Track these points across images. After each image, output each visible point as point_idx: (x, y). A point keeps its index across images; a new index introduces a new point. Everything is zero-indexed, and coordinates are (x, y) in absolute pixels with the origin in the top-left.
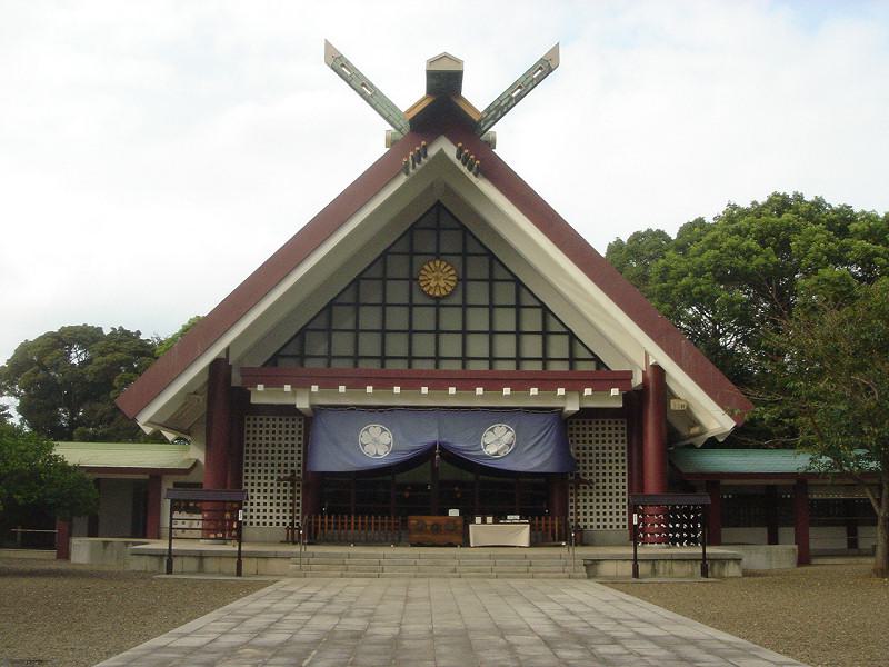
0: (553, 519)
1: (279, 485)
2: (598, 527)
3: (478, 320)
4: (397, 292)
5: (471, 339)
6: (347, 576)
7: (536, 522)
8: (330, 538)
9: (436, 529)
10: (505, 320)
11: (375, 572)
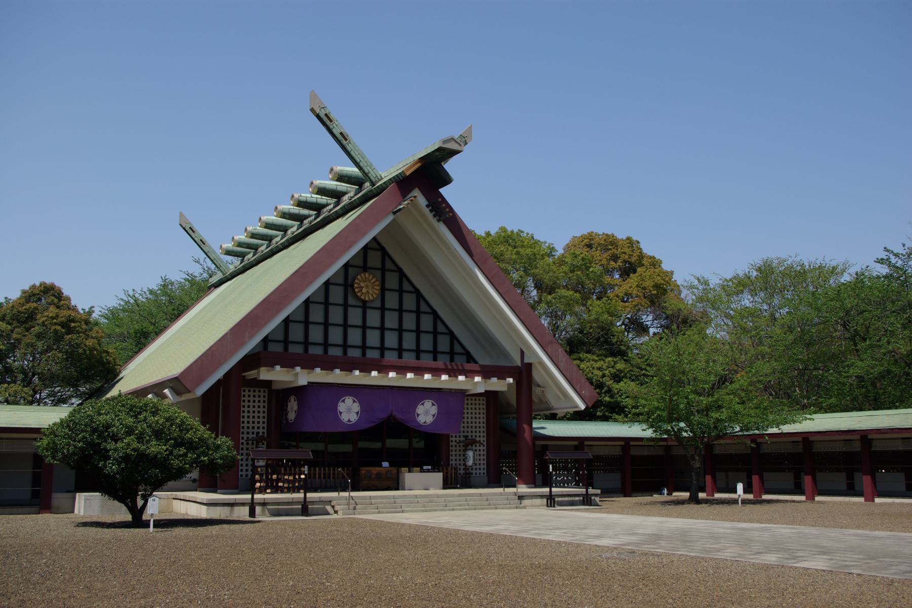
1: (248, 444)
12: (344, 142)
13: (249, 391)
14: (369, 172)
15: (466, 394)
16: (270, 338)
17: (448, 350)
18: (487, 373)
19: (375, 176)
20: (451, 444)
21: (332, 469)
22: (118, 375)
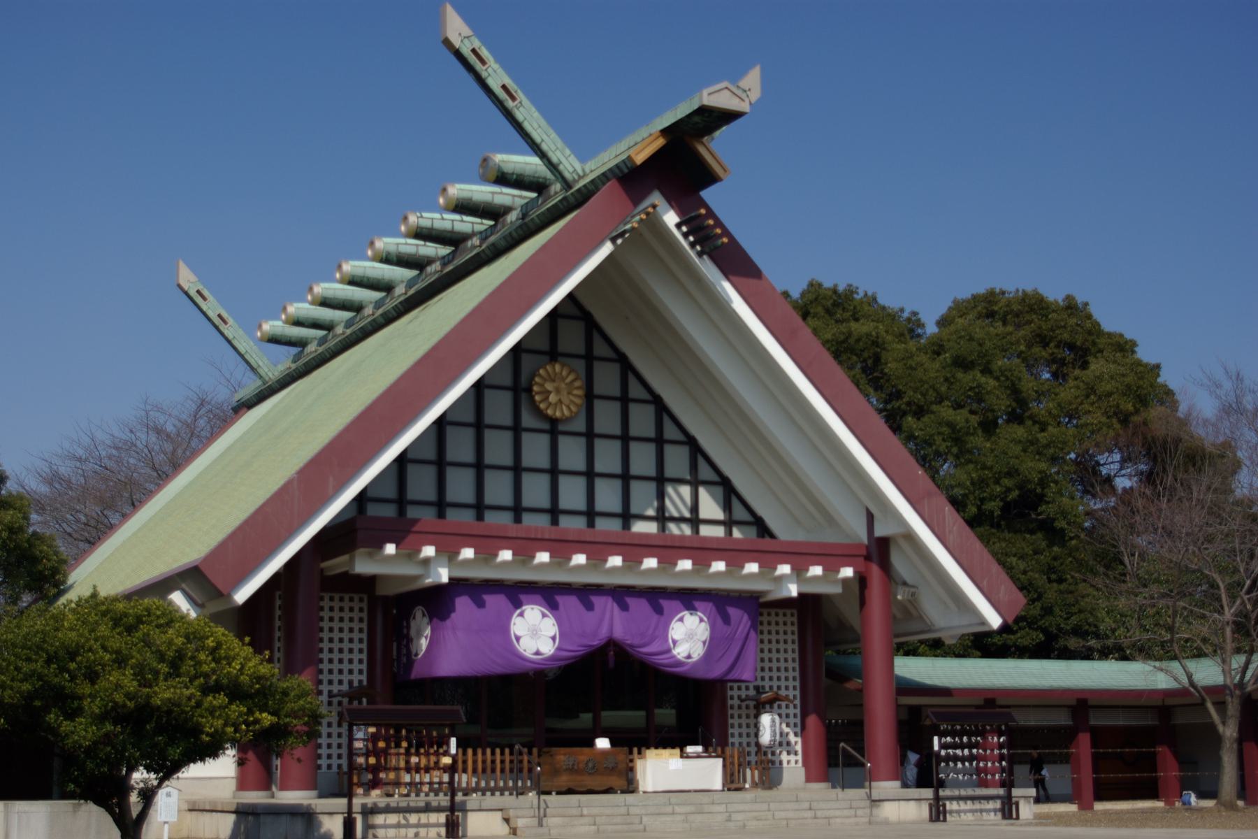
3: (608, 457)
13: (332, 599)
14: (561, 162)
15: (762, 600)
16: (487, 382)
18: (800, 556)
19: (571, 170)
20: (730, 702)
22: (64, 582)
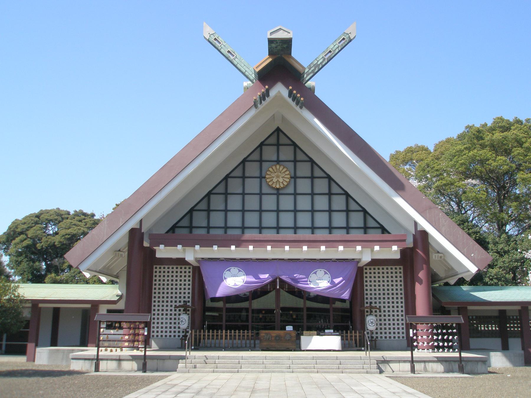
0: (355, 333)
1: (175, 310)
2: (386, 337)
4: (252, 185)
5: (317, 215)
6: (217, 372)
7: (345, 334)
8: (209, 345)
9: (278, 339)
10: (321, 203)
11: (237, 368)
12: (232, 58)
17: (362, 226)
21: (211, 331)
